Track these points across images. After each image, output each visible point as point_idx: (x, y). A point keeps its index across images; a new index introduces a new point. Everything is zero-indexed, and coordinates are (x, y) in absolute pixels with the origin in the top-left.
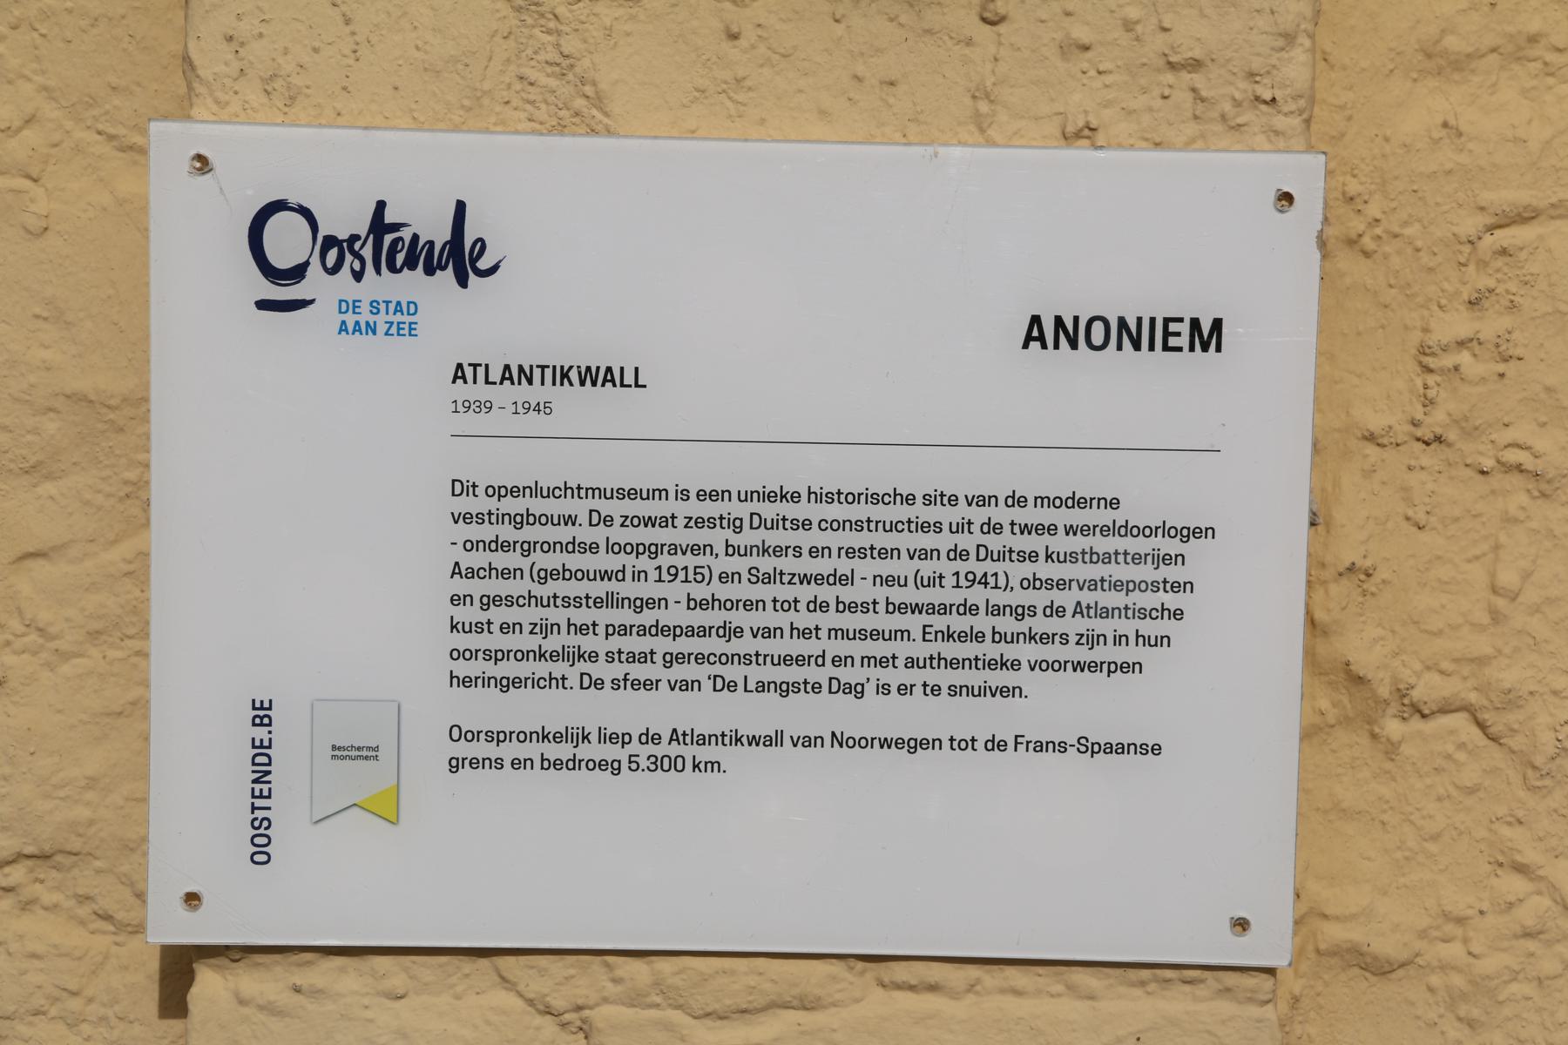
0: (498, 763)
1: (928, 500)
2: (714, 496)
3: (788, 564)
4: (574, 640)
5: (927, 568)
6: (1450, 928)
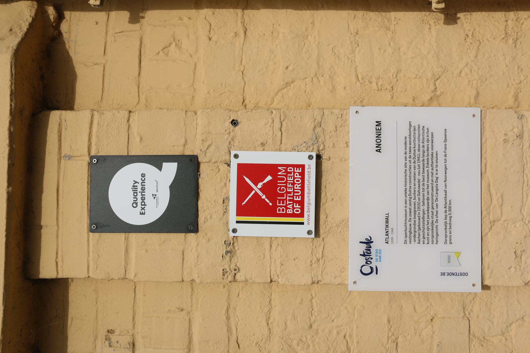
0: (450, 236)
1: (406, 167)
2: (406, 202)
3: (417, 190)
4: (430, 224)
5: (417, 167)
6: (471, 83)
